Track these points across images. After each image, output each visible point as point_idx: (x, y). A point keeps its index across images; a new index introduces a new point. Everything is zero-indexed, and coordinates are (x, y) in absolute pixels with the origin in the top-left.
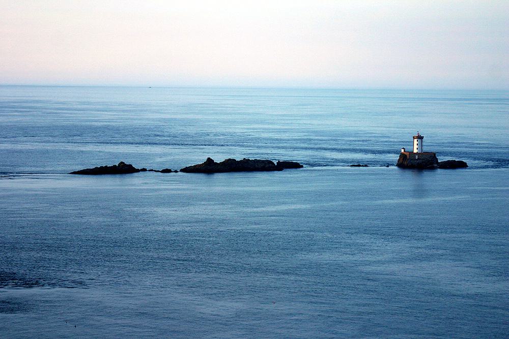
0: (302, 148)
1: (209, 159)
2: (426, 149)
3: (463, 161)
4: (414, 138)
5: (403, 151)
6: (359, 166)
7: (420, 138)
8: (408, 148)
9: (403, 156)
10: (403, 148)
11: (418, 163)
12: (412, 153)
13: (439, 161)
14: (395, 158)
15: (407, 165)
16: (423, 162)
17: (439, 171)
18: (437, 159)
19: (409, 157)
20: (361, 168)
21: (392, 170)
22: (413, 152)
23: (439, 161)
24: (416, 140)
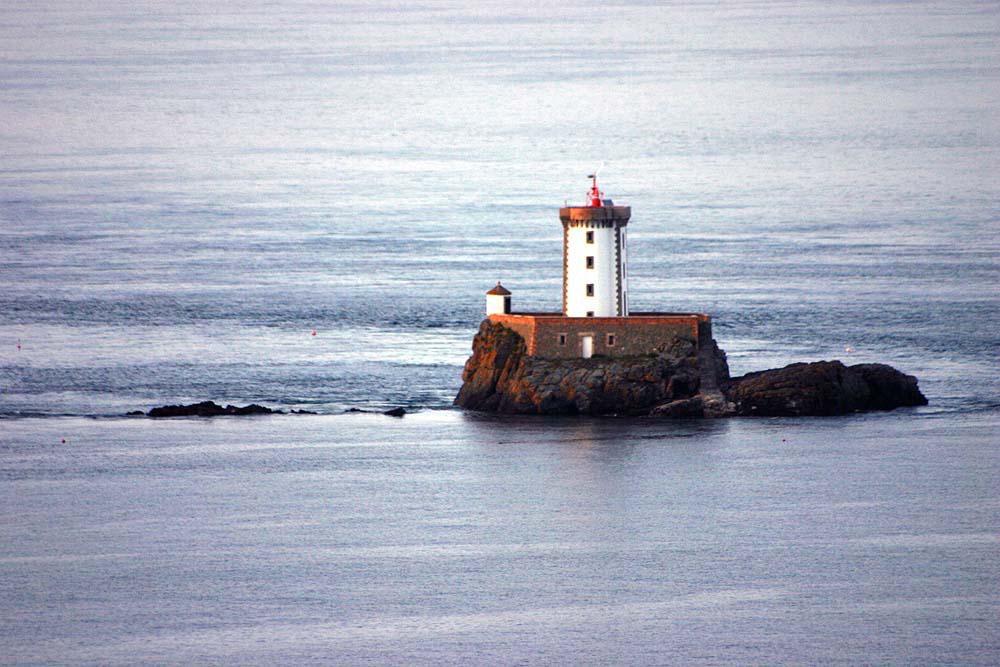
0: (728, 241)
1: (629, 209)
2: (656, 292)
3: (891, 364)
4: (567, 219)
5: (495, 306)
6: (207, 410)
7: (607, 216)
8: (534, 294)
9: (499, 345)
10: (499, 290)
11: (599, 389)
12: (553, 322)
13: (732, 374)
14: (455, 350)
15: (527, 396)
16: (627, 379)
17: (741, 438)
18: (722, 353)
19: (538, 343)
20: (222, 424)
21: (440, 433)
22: (561, 314)
23: (732, 374)
24: (578, 233)
